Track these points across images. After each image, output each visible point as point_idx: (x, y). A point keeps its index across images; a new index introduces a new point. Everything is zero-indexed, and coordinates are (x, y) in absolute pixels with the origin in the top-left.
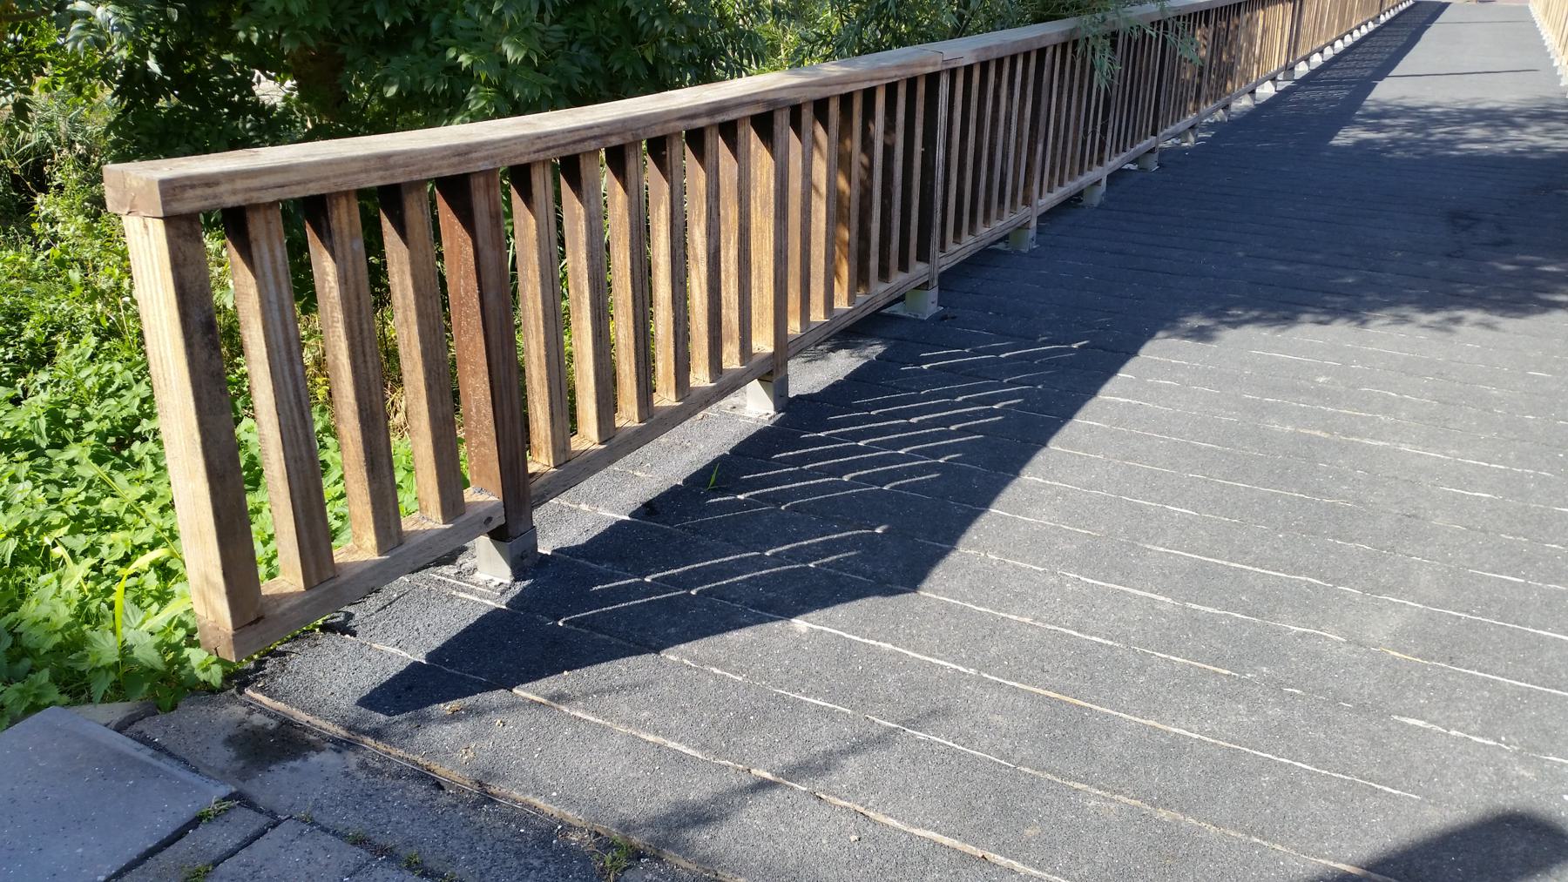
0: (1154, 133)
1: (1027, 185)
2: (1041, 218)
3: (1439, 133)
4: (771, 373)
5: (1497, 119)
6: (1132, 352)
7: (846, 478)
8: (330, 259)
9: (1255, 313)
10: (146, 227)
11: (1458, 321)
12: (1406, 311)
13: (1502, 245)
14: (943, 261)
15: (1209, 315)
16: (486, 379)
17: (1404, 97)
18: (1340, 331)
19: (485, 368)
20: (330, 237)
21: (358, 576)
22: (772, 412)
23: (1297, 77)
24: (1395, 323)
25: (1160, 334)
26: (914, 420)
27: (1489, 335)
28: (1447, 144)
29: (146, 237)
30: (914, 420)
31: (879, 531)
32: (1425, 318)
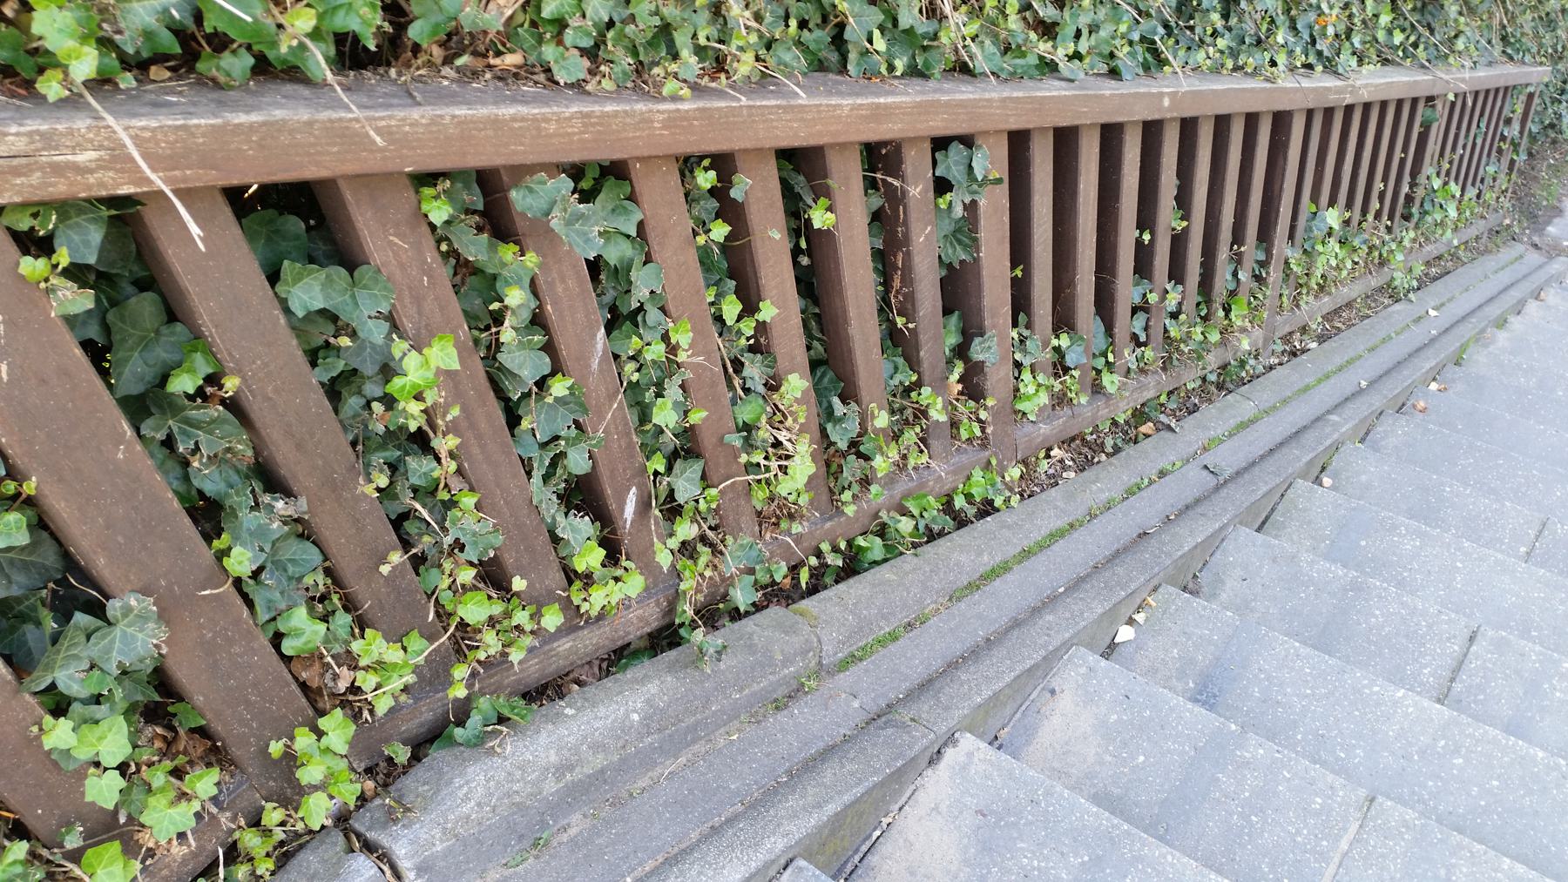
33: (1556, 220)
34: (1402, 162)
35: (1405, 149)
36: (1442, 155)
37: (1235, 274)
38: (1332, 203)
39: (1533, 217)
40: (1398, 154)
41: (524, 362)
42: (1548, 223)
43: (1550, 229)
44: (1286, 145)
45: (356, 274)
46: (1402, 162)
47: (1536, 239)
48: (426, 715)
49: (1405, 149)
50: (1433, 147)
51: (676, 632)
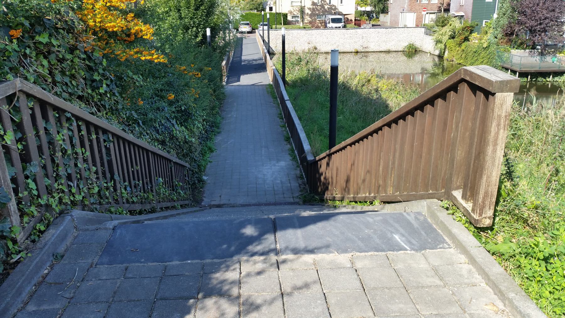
3: (251, 62)
5: (256, 60)
33: (203, 202)
34: (169, 175)
35: (169, 172)
36: (176, 178)
37: (147, 187)
38: (159, 177)
39: (198, 202)
40: (168, 174)
41: (148, 207)
42: (202, 202)
43: (202, 204)
44: (149, 158)
45: (259, 301)
46: (169, 175)
47: (200, 206)
48: (232, 285)
49: (169, 172)
50: (174, 177)
51: (6, 238)
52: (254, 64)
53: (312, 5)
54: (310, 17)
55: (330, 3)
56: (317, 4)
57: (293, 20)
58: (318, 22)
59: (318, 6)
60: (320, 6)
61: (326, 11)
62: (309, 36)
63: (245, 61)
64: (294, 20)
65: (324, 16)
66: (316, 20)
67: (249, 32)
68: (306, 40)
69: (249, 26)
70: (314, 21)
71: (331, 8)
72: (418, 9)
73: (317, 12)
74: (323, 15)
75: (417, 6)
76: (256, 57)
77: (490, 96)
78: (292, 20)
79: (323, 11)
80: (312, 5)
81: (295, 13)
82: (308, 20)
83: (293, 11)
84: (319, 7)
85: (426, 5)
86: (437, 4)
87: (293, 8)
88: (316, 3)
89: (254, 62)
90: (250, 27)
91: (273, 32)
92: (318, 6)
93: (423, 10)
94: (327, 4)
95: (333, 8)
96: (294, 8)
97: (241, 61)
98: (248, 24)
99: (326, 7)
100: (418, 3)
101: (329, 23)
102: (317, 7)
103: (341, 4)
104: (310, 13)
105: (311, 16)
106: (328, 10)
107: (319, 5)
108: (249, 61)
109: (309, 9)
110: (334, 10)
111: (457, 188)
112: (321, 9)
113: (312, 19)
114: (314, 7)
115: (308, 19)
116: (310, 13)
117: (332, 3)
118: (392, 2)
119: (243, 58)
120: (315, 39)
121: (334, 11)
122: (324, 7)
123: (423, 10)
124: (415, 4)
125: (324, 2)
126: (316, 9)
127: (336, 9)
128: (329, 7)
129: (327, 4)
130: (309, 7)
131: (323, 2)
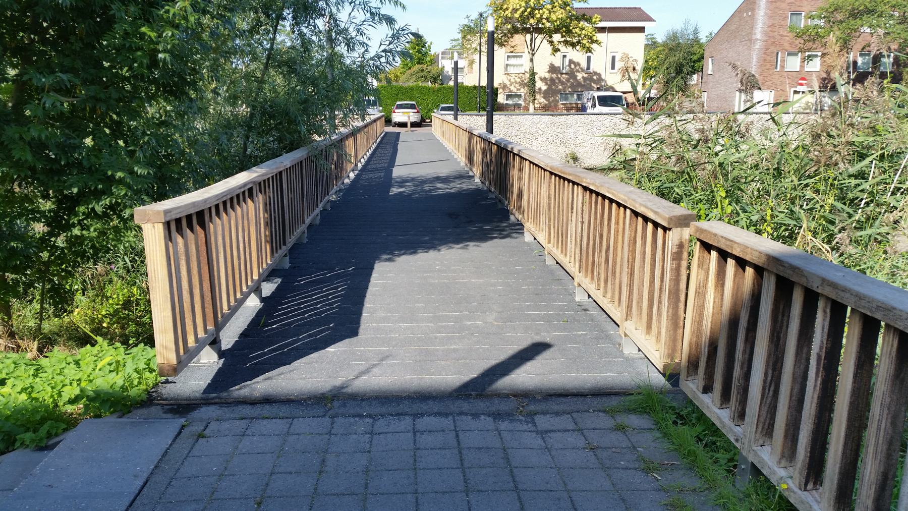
0: (328, 195)
1: (303, 214)
2: (307, 228)
3: (427, 187)
4: (257, 290)
5: (446, 180)
6: (372, 269)
7: (306, 316)
8: (181, 238)
9: (403, 252)
10: (154, 226)
11: (467, 245)
12: (451, 245)
13: (470, 222)
14: (289, 245)
15: (388, 254)
16: (209, 282)
17: (410, 174)
18: (432, 254)
19: (208, 278)
20: (182, 230)
21: (194, 350)
22: (259, 303)
23: (359, 169)
24: (449, 249)
25: (377, 262)
26: (314, 297)
27: (479, 248)
28: (430, 191)
29: (153, 230)
30: (314, 297)
31: (331, 326)
32: (458, 246)
52: (440, 192)
53: (549, 72)
54: (544, 98)
55: (588, 68)
56: (560, 70)
57: (508, 102)
58: (562, 106)
59: (562, 74)
60: (566, 74)
61: (579, 84)
62: (559, 130)
63: (403, 182)
64: (510, 102)
65: (575, 96)
66: (558, 102)
67: (414, 125)
68: (550, 139)
69: (415, 111)
70: (552, 104)
71: (592, 80)
72: (778, 83)
73: (560, 87)
74: (572, 94)
75: (777, 77)
76: (444, 170)
77: (728, 259)
78: (506, 102)
79: (572, 84)
80: (549, 72)
81: (512, 88)
82: (540, 103)
83: (508, 83)
84: (564, 76)
85: (794, 74)
86: (818, 74)
87: (509, 77)
88: (559, 67)
89: (439, 185)
90: (418, 112)
91: (472, 120)
92: (562, 74)
93: (800, 82)
94: (583, 70)
95: (595, 77)
96: (512, 78)
97: (388, 181)
98: (412, 107)
99: (580, 76)
100: (778, 70)
101: (594, 106)
102: (559, 76)
103: (613, 71)
104: (544, 87)
105: (546, 95)
106: (583, 83)
107: (564, 72)
108: (420, 182)
109: (544, 80)
110: (595, 82)
111: (178, 81)
112: (568, 80)
113: (548, 100)
114: (554, 76)
115: (540, 101)
116: (544, 87)
117: (593, 68)
118: (710, 72)
119: (398, 172)
120: (573, 137)
121: (597, 84)
122: (575, 77)
123: (800, 82)
124: (771, 72)
125: (575, 66)
126: (557, 81)
127: (600, 79)
128: (586, 75)
129: (583, 70)
130: (543, 77)
131: (573, 66)
